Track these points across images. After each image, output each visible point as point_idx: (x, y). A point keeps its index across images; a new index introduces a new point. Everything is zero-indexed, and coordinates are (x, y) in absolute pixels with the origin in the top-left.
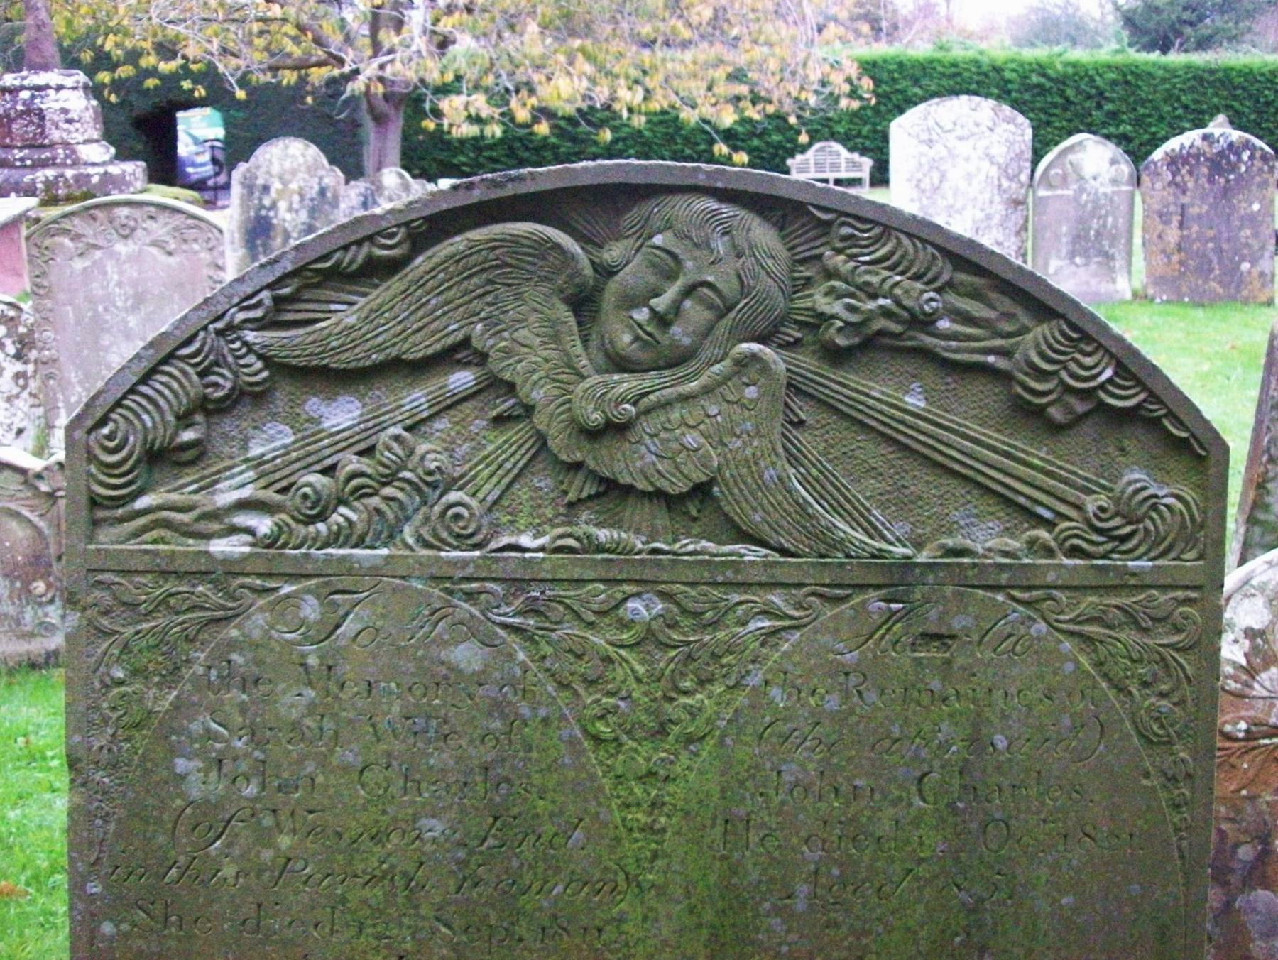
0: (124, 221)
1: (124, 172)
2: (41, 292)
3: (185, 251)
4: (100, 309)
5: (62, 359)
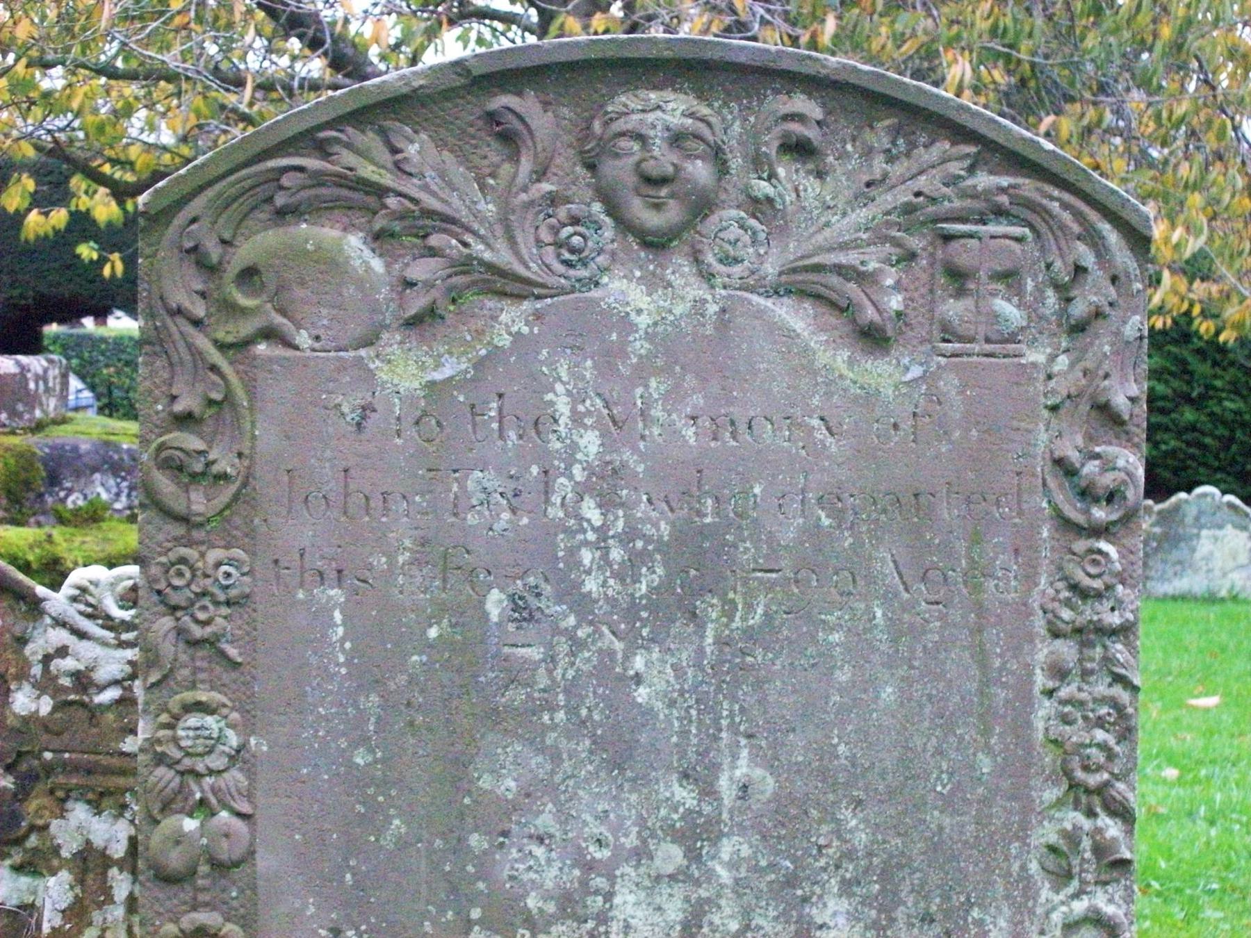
0: (663, 158)
1: (24, 369)
2: (199, 502)
3: (949, 333)
4: (495, 604)
5: (265, 862)
